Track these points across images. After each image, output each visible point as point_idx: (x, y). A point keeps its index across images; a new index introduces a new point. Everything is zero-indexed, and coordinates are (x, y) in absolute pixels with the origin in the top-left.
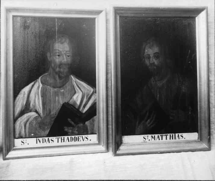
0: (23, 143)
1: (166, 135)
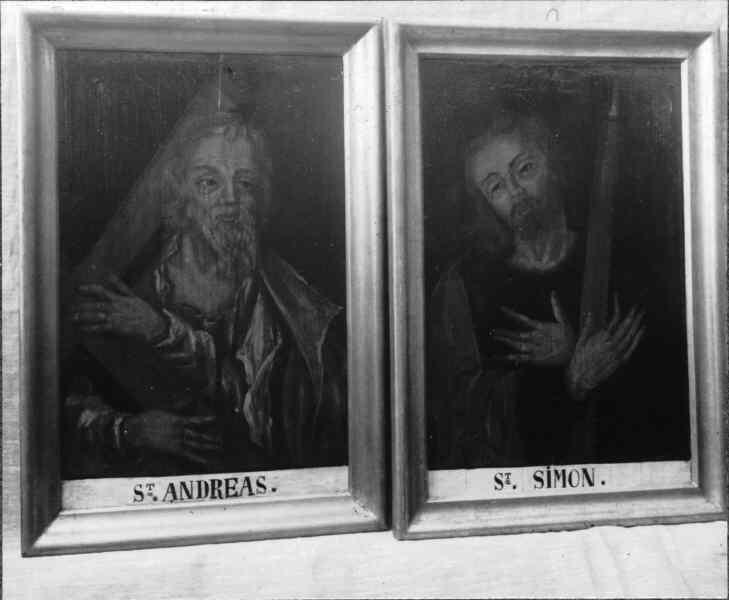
0: (139, 497)
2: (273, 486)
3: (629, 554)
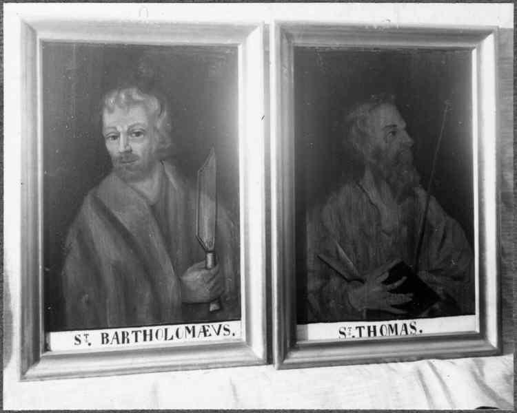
1: (360, 328)
2: (421, 329)
3: (448, 376)
